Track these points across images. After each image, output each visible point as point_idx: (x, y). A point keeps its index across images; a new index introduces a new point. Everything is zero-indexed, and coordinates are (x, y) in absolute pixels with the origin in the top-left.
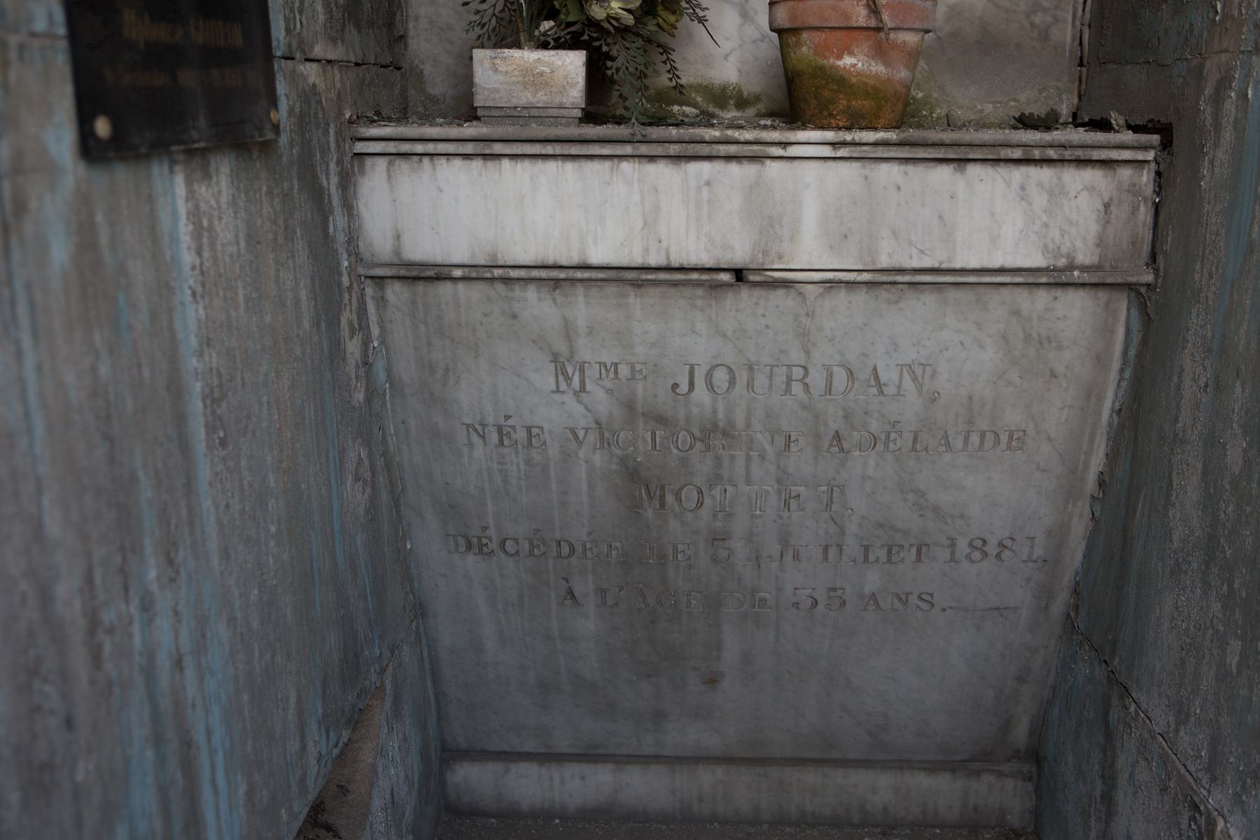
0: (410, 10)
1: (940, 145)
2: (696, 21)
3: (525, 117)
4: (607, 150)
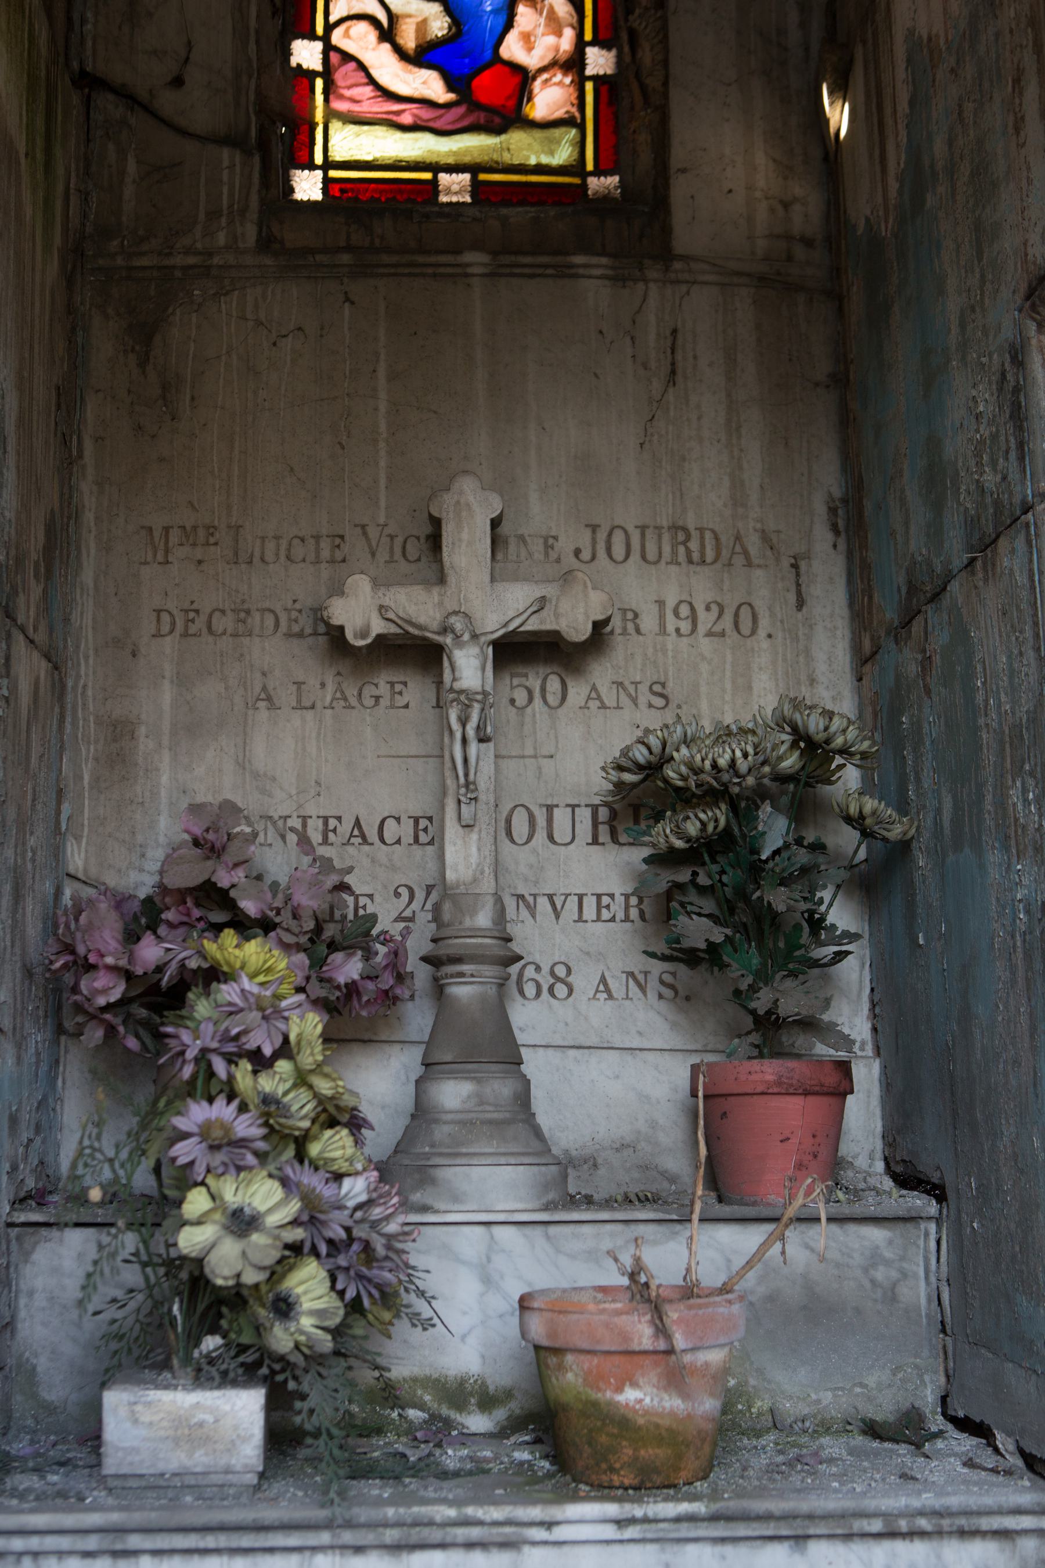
0: (22, 1282)
1: (767, 1517)
2: (420, 1328)
3: (175, 1487)
4: (293, 1540)
